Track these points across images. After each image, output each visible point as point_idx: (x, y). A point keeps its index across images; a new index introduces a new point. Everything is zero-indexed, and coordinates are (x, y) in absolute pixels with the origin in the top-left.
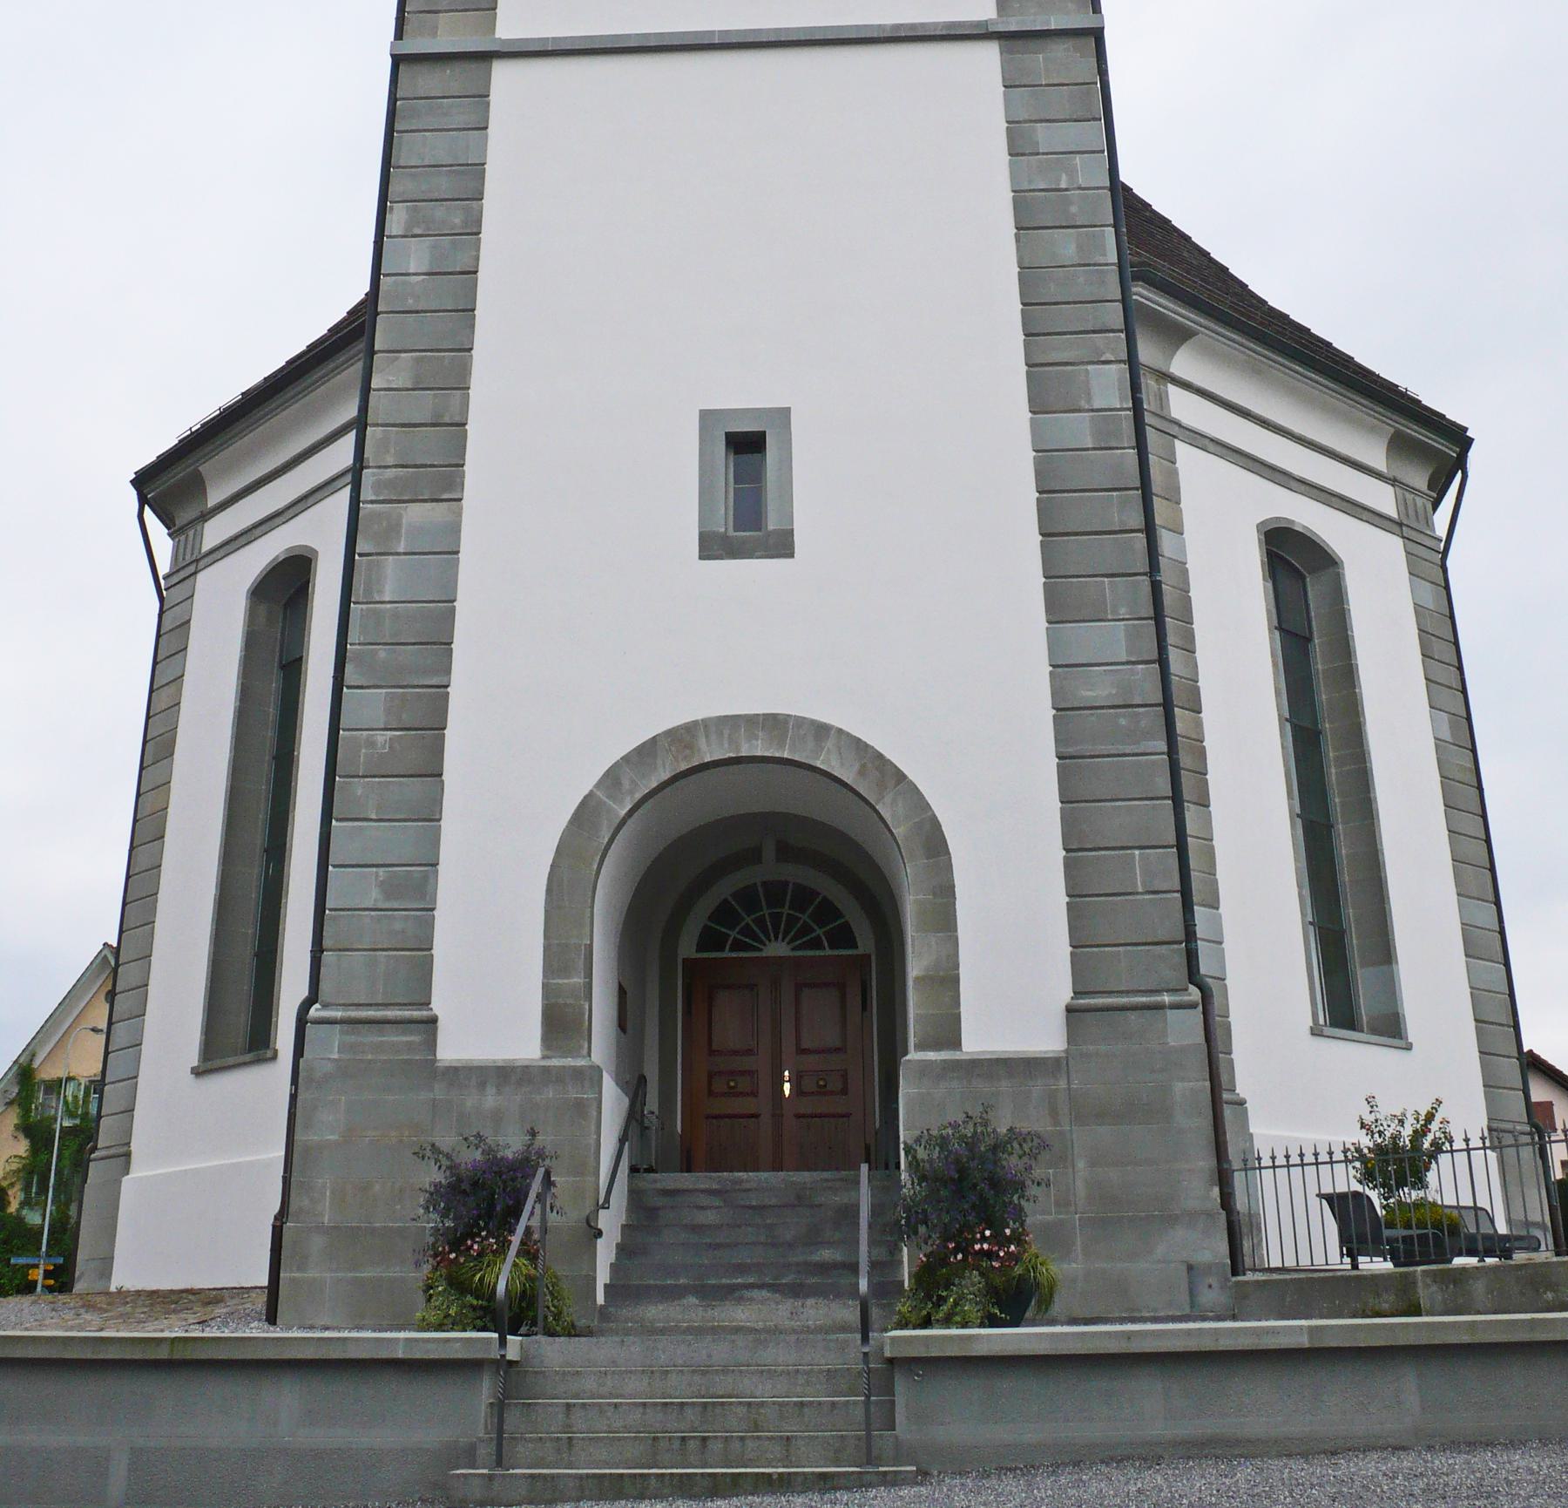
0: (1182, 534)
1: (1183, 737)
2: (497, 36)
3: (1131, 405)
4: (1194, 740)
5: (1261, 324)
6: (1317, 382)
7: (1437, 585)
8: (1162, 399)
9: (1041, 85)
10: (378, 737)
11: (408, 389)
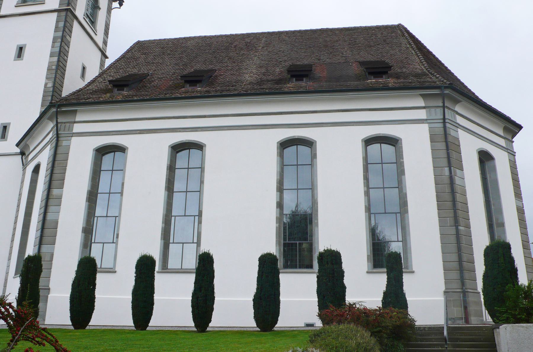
0: (463, 171)
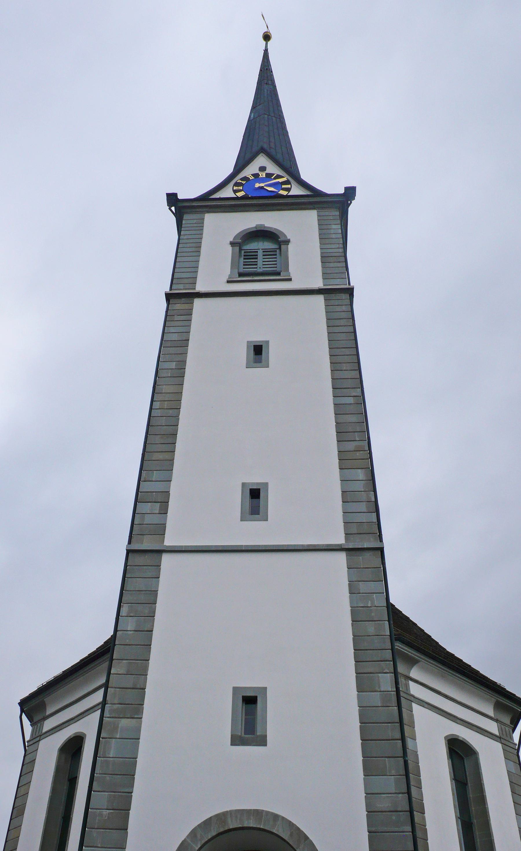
0: (416, 740)
1: (418, 824)
2: (165, 544)
3: (395, 690)
4: (422, 825)
5: (444, 658)
6: (464, 680)
7: (516, 763)
8: (407, 686)
9: (361, 568)
10: (104, 812)
11: (124, 674)
